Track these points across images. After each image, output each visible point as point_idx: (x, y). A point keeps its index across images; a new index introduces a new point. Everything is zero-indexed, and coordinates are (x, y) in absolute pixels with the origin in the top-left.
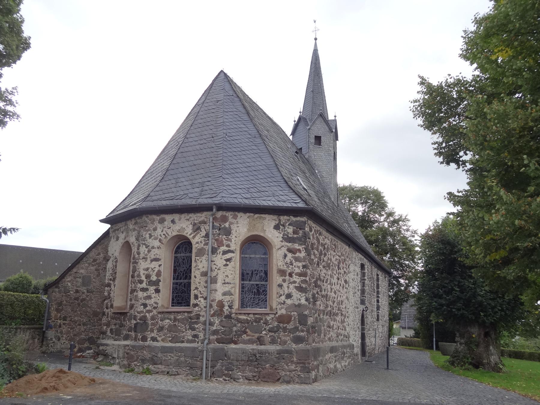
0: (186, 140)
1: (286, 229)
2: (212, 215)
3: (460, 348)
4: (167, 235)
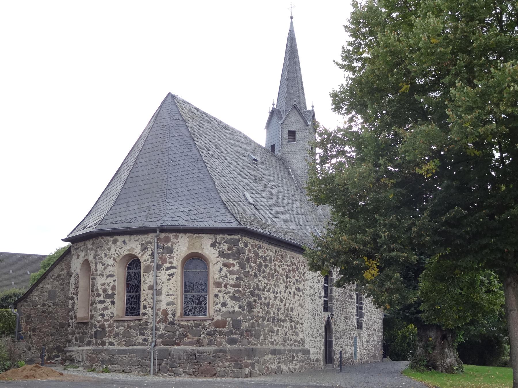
1: (222, 246)
2: (157, 236)
4: (119, 254)
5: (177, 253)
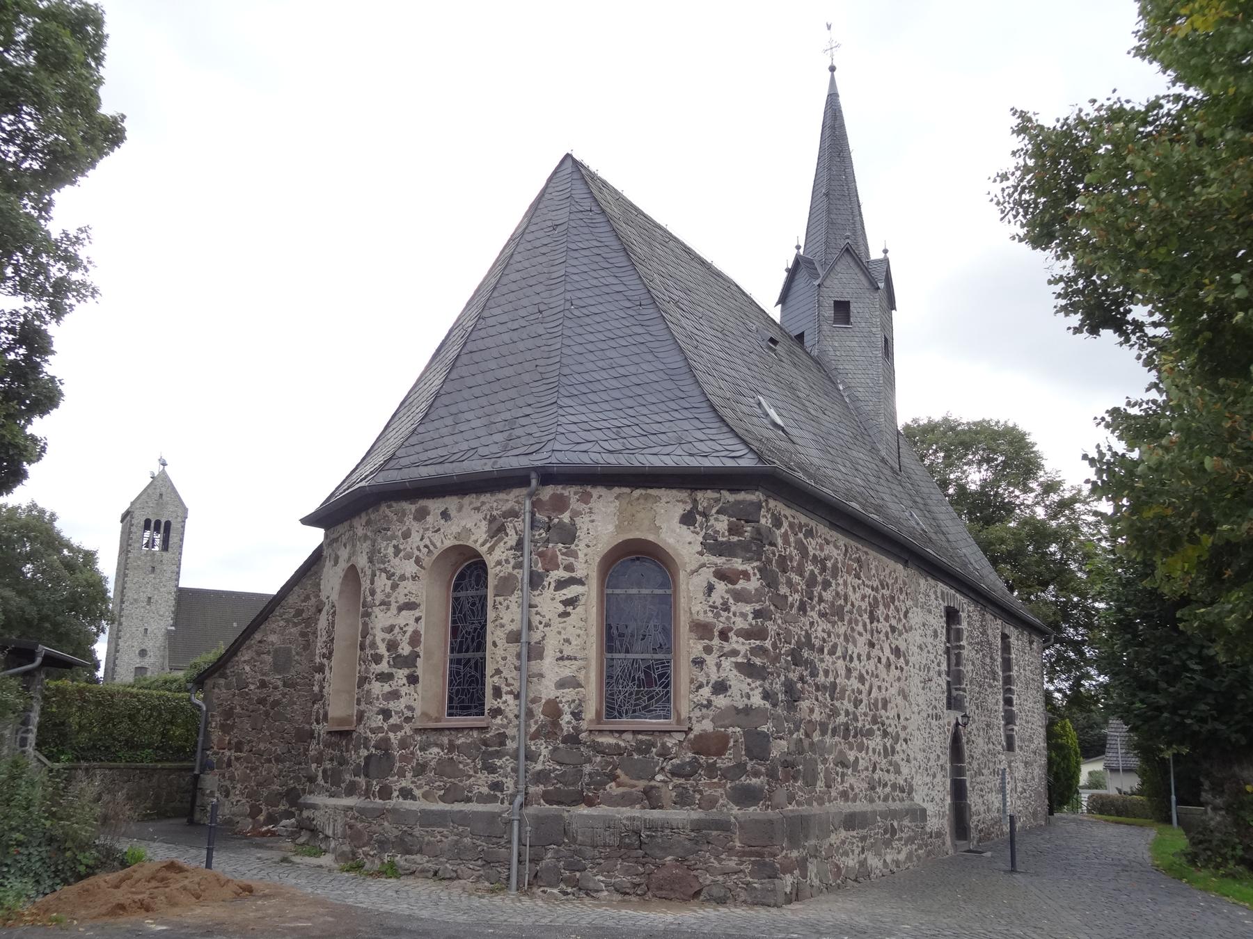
0: (482, 324)
1: (712, 522)
2: (530, 495)
3: (1212, 819)
4: (431, 548)
5: (586, 541)
